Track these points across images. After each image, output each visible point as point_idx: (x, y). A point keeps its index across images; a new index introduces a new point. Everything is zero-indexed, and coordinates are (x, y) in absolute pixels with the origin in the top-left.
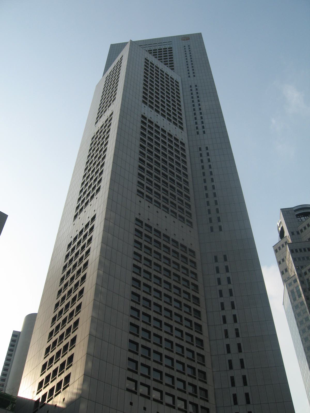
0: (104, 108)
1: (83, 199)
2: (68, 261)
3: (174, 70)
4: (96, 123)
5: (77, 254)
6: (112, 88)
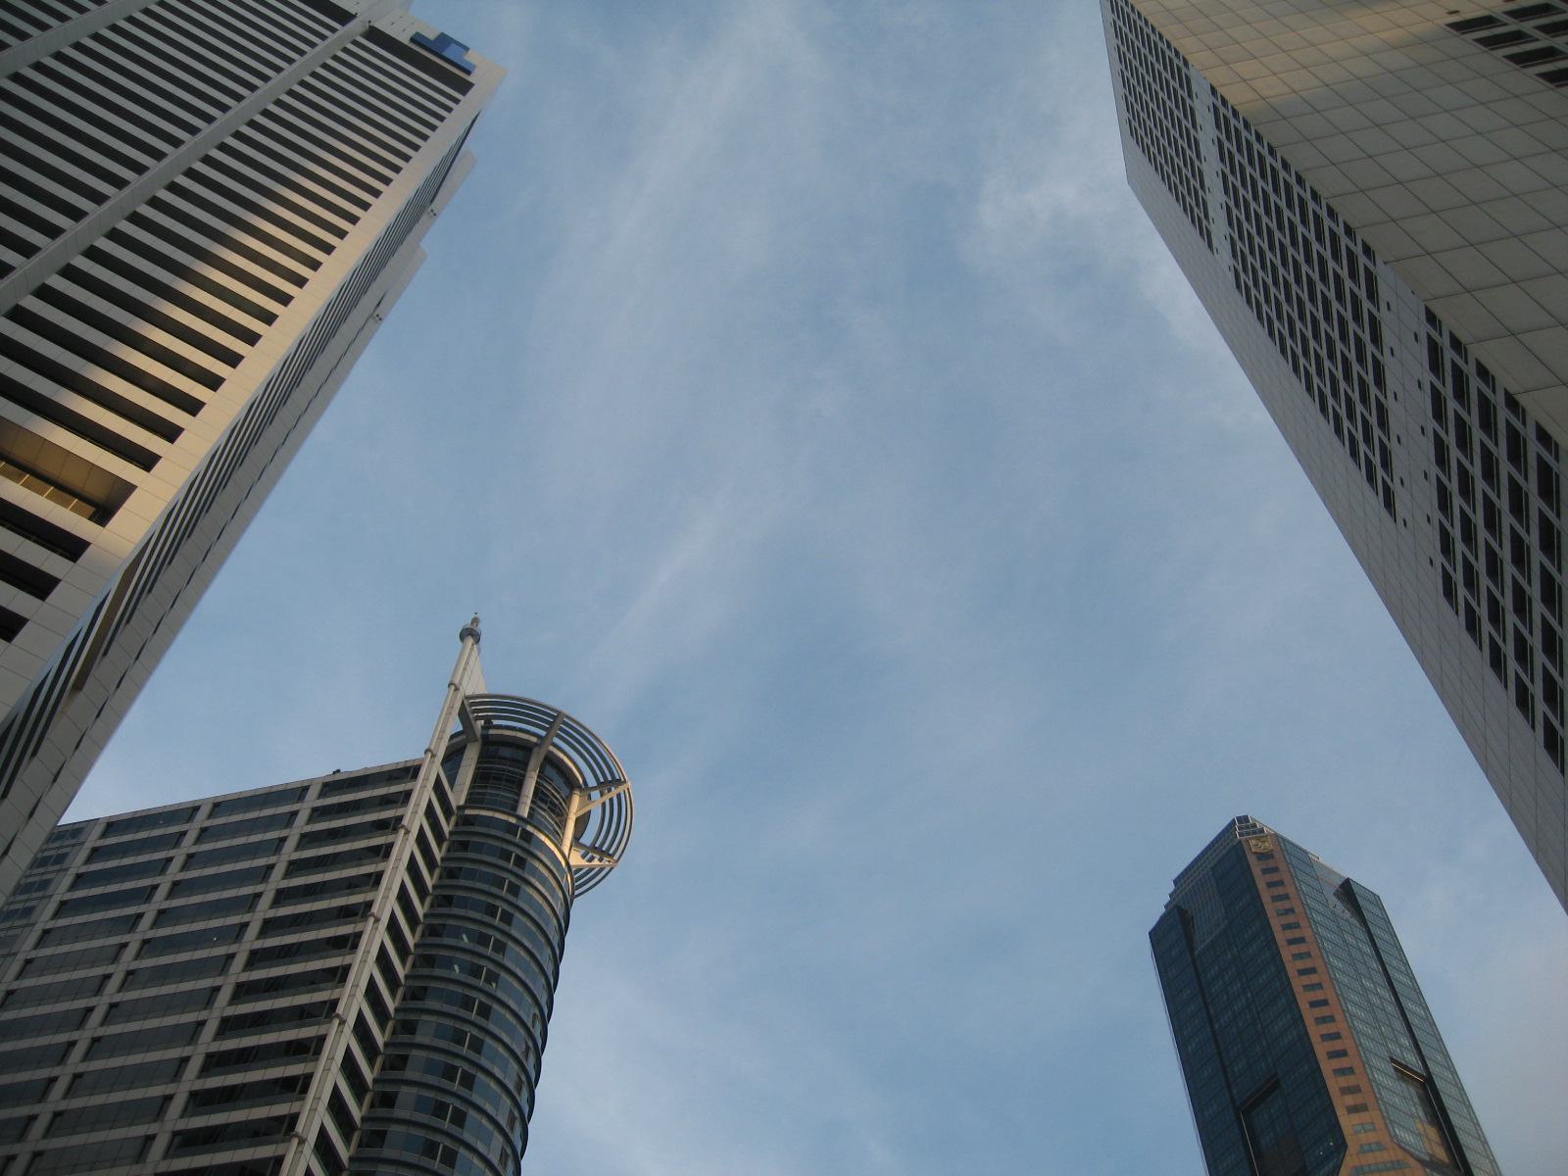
4: (1389, 503)
6: (1262, 299)
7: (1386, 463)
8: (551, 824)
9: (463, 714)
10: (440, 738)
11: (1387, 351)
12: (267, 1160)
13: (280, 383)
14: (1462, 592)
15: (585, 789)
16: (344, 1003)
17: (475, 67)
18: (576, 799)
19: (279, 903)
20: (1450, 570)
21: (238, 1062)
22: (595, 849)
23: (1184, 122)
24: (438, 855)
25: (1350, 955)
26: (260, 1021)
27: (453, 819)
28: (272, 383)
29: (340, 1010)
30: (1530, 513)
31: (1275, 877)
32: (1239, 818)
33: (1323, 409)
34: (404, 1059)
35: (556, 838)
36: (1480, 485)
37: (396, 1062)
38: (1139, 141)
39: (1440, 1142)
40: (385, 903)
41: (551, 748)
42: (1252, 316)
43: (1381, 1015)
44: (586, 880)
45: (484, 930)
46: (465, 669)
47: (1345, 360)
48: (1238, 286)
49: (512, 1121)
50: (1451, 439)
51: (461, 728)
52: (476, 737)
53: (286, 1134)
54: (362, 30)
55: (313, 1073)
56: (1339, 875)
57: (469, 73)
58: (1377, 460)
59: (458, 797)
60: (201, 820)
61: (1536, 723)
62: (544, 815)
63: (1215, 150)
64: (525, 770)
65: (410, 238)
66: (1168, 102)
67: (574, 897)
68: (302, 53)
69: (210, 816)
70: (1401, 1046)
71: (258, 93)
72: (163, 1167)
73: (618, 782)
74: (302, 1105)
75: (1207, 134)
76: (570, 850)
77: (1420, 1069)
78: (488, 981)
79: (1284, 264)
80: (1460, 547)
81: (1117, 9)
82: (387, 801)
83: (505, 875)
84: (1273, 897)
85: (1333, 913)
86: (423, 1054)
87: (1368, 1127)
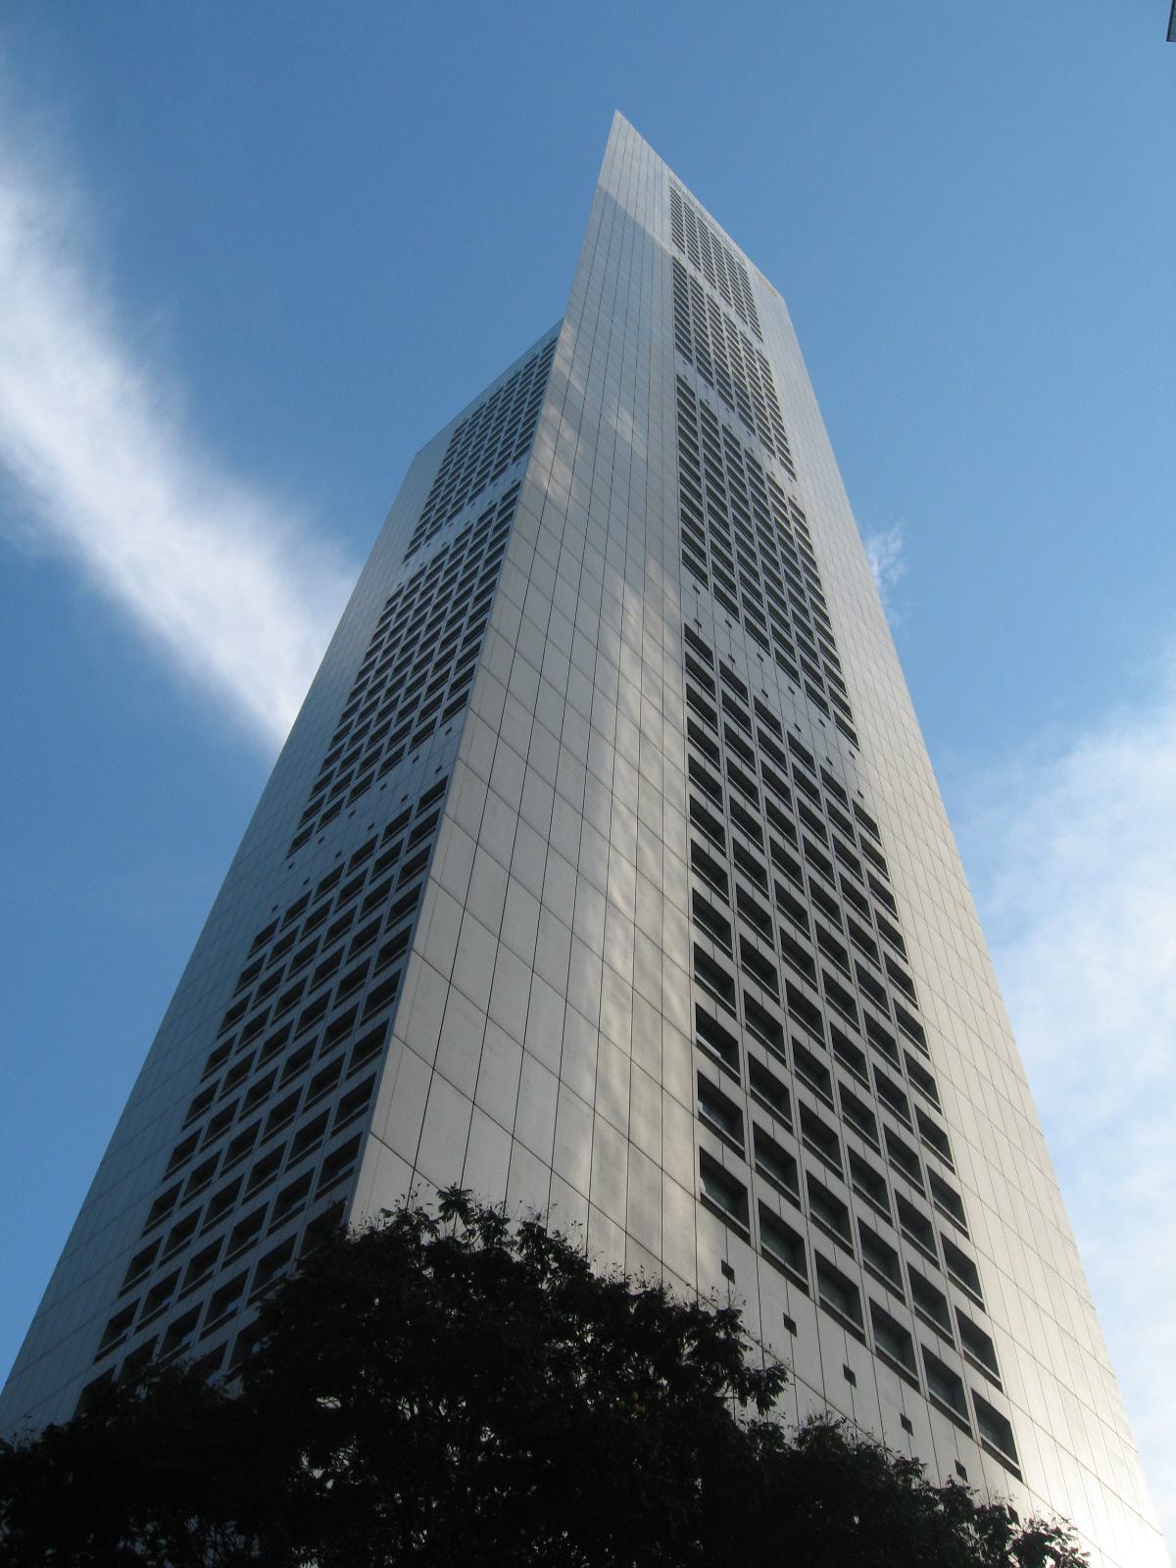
0: (365, 740)
1: (204, 1165)
2: (142, 1292)
3: (959, 1481)
4: (298, 843)
6: (392, 627)
7: (327, 818)
11: (414, 755)
14: (268, 949)
20: (311, 900)
33: (328, 762)
47: (378, 753)
48: (390, 602)
50: (379, 853)
58: (325, 809)
61: (207, 1080)
63: (485, 509)
79: (430, 626)
80: (301, 921)
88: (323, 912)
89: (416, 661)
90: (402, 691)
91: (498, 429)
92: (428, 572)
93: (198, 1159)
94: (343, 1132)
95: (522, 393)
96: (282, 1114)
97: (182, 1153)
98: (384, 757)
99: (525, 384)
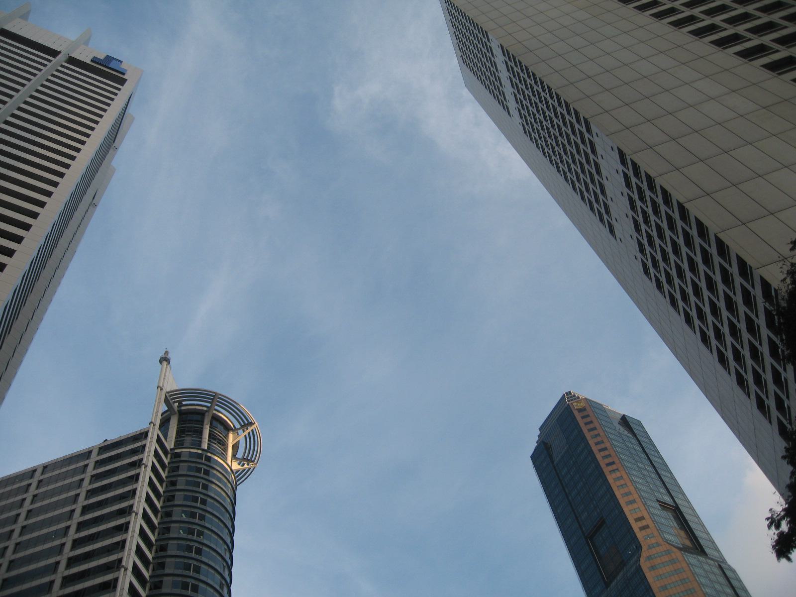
0: (582, 176)
4: (612, 231)
5: (755, 354)
6: (537, 137)
7: (608, 212)
8: (219, 450)
9: (167, 401)
10: (156, 416)
11: (600, 157)
12: (111, 581)
13: (35, 273)
14: (652, 271)
15: (235, 430)
16: (132, 526)
17: (126, 70)
18: (231, 436)
19: (75, 547)
20: (641, 239)
21: (105, 476)
22: (242, 461)
23: (488, 54)
24: (166, 461)
25: (630, 453)
26: (88, 556)
27: (169, 456)
28: (34, 261)
29: (124, 563)
30: (739, 313)
31: (588, 420)
32: (567, 393)
33: (583, 198)
34: (173, 496)
35: (223, 457)
36: (648, 193)
37: (170, 498)
38: (468, 65)
39: (686, 537)
40: (140, 505)
41: (214, 412)
42: (534, 146)
43: (649, 480)
44: (241, 476)
45: (194, 494)
46: (164, 378)
47: (590, 173)
49: (221, 586)
50: (636, 197)
51: (167, 409)
52: (174, 411)
53: (129, 513)
54: (65, 59)
55: (136, 488)
56: (620, 414)
57: (124, 74)
58: (603, 211)
59: (170, 444)
60: (38, 476)
62: (217, 447)
63: (504, 66)
64: (203, 425)
65: (105, 162)
66: (483, 59)
67: (237, 485)
68: (40, 70)
69: (42, 473)
70: (661, 493)
71: (14, 99)
72: (61, 593)
73: (251, 424)
74: (119, 574)
75: (500, 59)
76: (232, 462)
77: (672, 503)
78: (198, 536)
80: (648, 249)
81: (451, 4)
82: (134, 452)
83: (199, 480)
84: (588, 430)
85: (619, 433)
86: (170, 578)
87: (650, 536)
88: (649, 237)
89: (557, 134)
90: (577, 157)
91: (471, 43)
92: (521, 108)
93: (729, 355)
94: (732, 262)
95: (460, 22)
96: (731, 305)
97: (722, 359)
98: (594, 171)
99: (457, 19)
